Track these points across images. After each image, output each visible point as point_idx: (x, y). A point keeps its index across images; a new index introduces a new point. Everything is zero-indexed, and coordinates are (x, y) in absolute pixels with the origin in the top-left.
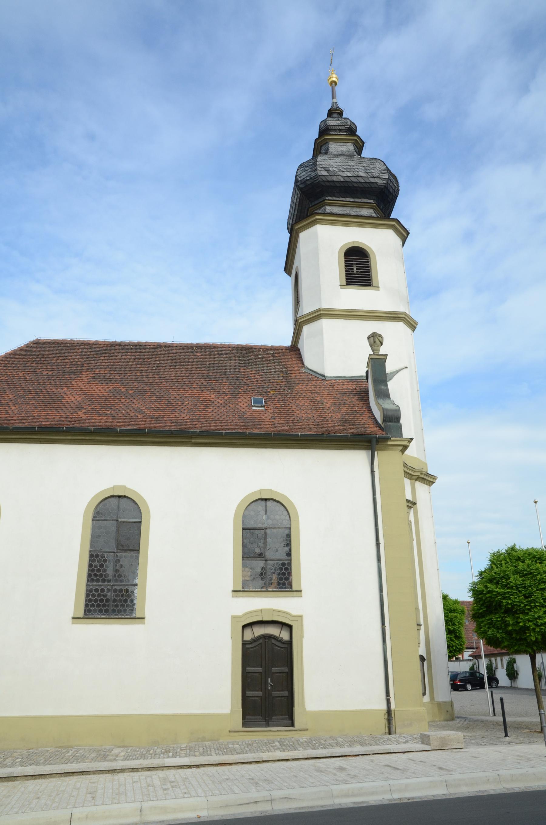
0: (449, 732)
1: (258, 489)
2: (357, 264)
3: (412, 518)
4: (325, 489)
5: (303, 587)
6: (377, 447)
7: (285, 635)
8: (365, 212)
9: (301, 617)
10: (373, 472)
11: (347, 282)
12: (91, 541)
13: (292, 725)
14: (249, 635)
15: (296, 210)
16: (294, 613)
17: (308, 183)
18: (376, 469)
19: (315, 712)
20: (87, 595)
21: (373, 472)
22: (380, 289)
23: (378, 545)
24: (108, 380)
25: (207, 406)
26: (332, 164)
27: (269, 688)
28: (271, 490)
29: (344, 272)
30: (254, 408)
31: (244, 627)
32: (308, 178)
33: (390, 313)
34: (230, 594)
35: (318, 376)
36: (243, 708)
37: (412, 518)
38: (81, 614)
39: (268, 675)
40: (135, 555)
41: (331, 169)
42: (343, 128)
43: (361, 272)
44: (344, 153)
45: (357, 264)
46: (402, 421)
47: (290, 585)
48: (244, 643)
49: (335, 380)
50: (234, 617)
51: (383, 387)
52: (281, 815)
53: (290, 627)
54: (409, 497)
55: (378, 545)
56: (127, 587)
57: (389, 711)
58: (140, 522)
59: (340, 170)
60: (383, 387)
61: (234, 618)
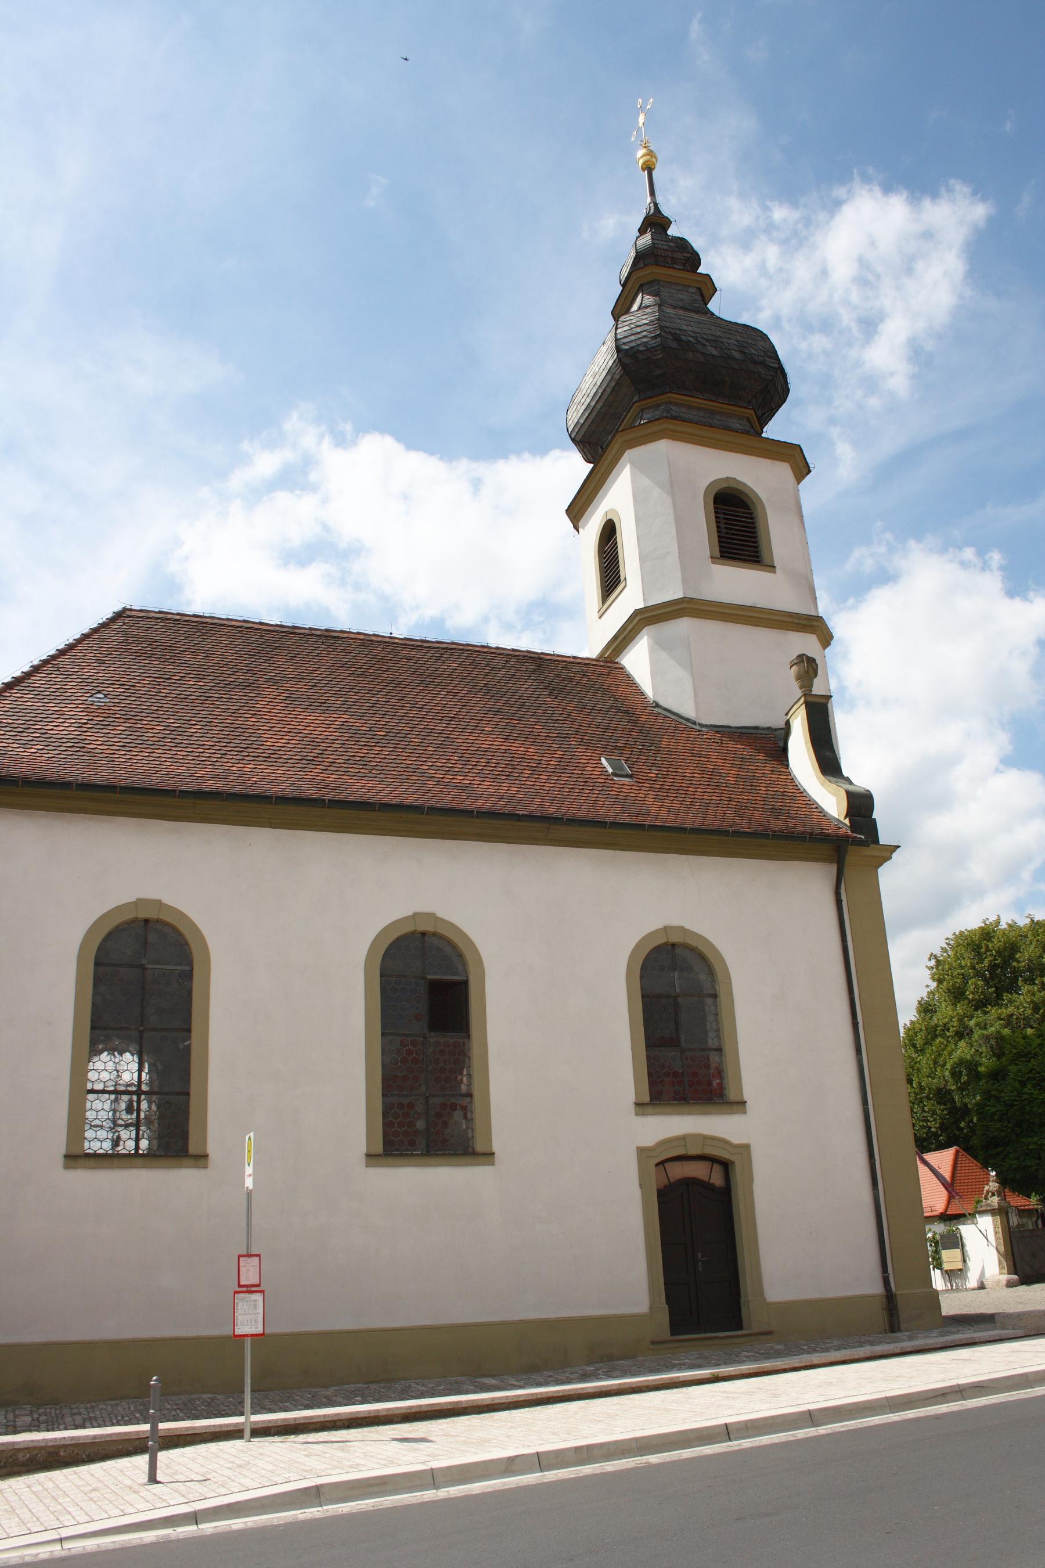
1: (660, 926)
2: (725, 519)
4: (760, 926)
8: (735, 424)
9: (747, 1147)
11: (721, 551)
12: (650, 1075)
13: (739, 1326)
15: (603, 400)
16: (736, 1141)
17: (641, 357)
18: (843, 897)
19: (779, 1303)
20: (385, 1115)
22: (778, 570)
26: (685, 327)
27: (701, 1269)
28: (683, 928)
32: (641, 348)
34: (632, 1108)
36: (667, 1303)
38: (380, 1149)
40: (461, 1041)
43: (732, 529)
44: (687, 306)
45: (725, 519)
48: (661, 1193)
51: (827, 753)
52: (668, 1463)
56: (453, 1100)
57: (890, 1297)
59: (699, 342)
60: (827, 753)
61: (642, 1151)
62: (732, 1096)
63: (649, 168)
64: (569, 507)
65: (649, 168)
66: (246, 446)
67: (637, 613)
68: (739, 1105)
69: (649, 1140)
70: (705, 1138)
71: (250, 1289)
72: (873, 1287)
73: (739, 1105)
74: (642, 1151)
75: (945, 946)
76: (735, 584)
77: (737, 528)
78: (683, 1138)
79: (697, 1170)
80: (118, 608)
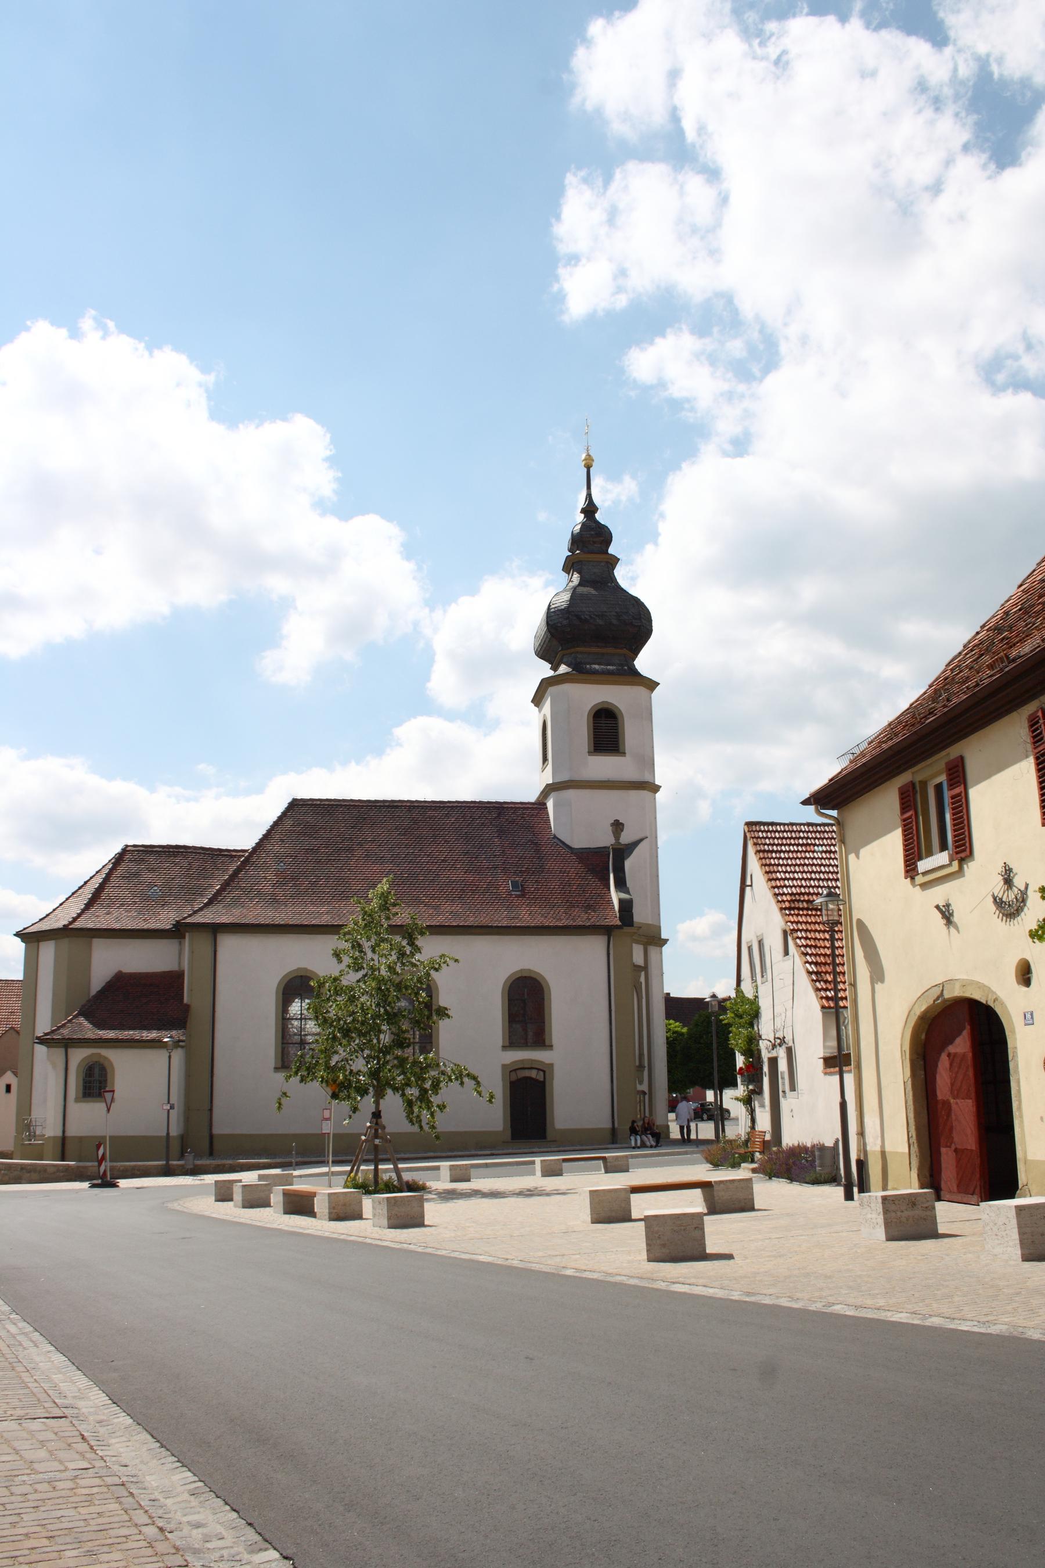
3: (642, 979)
4: (574, 972)
7: (541, 1078)
9: (552, 1065)
14: (514, 1078)
18: (611, 952)
37: (642, 979)
48: (511, 1083)
57: (613, 1129)
61: (504, 1066)
62: (547, 1043)
63: (588, 467)
64: (149, 850)
65: (588, 467)
66: (565, 622)
67: (548, 785)
68: (550, 1047)
69: (508, 1062)
70: (532, 1061)
71: (327, 1119)
72: (609, 1125)
73: (550, 1047)
74: (504, 1066)
75: (299, 1077)
76: (604, 766)
77: (606, 731)
78: (522, 1061)
79: (533, 1074)
80: (290, 800)
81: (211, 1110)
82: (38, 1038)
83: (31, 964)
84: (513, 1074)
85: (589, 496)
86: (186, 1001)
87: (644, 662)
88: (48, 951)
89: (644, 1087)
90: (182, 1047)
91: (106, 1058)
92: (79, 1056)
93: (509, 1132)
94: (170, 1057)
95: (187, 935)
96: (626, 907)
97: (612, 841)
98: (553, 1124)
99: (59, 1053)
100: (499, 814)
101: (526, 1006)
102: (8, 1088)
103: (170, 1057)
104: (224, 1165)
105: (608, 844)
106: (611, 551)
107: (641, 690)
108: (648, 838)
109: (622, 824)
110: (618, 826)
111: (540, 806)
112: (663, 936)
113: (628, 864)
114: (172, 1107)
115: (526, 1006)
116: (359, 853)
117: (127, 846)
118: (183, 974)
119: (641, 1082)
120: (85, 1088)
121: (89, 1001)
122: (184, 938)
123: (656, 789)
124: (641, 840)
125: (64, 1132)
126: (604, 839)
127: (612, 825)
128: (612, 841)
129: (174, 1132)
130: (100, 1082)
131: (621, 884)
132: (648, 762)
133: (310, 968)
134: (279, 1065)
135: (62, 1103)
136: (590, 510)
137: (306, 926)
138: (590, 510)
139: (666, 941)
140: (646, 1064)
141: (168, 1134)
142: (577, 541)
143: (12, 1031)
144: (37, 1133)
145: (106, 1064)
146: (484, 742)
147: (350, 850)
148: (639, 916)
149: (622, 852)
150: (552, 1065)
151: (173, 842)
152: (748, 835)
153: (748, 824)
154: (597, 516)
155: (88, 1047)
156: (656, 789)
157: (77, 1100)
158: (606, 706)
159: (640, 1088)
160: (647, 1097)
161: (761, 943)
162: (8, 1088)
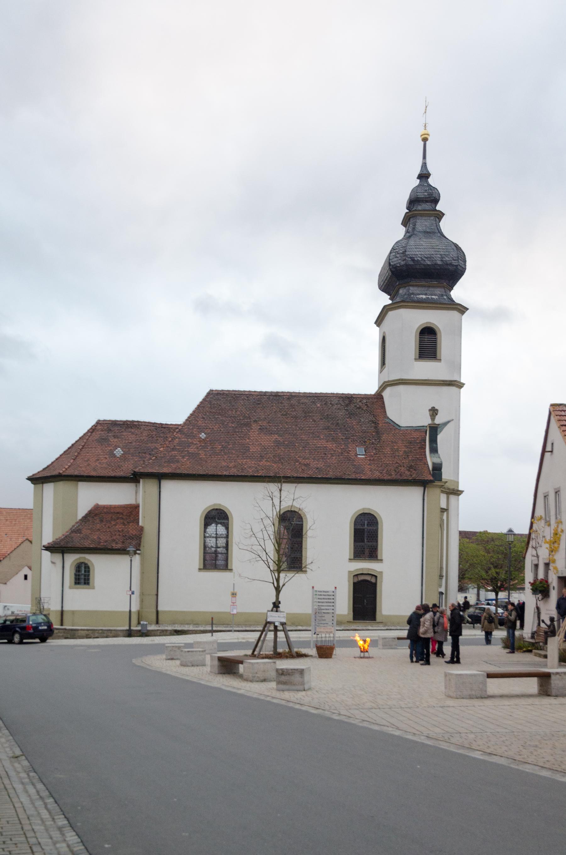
0: (560, 780)
3: (445, 517)
4: (398, 510)
5: (384, 558)
6: (427, 486)
7: (373, 580)
10: (424, 499)
13: (375, 620)
14: (356, 580)
16: (378, 570)
18: (426, 498)
21: (424, 499)
22: (442, 361)
23: (423, 538)
24: (271, 433)
25: (332, 455)
26: (417, 253)
29: (418, 345)
30: (359, 456)
31: (354, 576)
32: (398, 265)
33: (446, 381)
35: (395, 425)
37: (445, 517)
39: (365, 599)
41: (416, 259)
42: (429, 199)
46: (443, 470)
47: (377, 557)
48: (354, 584)
49: (407, 430)
50: (349, 572)
53: (376, 577)
54: (444, 506)
55: (423, 538)
58: (302, 524)
61: (350, 572)
62: (379, 558)
64: (114, 423)
66: (403, 263)
69: (352, 569)
74: (350, 572)
77: (428, 343)
81: (157, 595)
82: (44, 546)
83: (39, 499)
84: (356, 578)
85: (424, 165)
86: (140, 524)
87: (458, 293)
88: (49, 489)
89: (442, 590)
90: (139, 554)
91: (89, 560)
92: (71, 559)
93: (351, 616)
94: (131, 561)
95: (141, 481)
96: (438, 468)
97: (430, 421)
98: (381, 611)
99: (58, 558)
100: (350, 402)
101: (366, 535)
102: (26, 577)
103: (131, 561)
104: (166, 631)
105: (426, 424)
106: (438, 208)
107: (455, 313)
108: (454, 420)
109: (437, 410)
110: (434, 412)
111: (378, 397)
112: (460, 488)
113: (440, 437)
114: (133, 593)
115: (366, 535)
116: (255, 426)
117: (99, 421)
118: (139, 506)
119: (440, 586)
120: (76, 579)
121: (77, 523)
122: (139, 482)
123: (460, 385)
124: (449, 422)
125: (62, 607)
126: (425, 421)
127: (430, 410)
128: (430, 421)
129: (134, 609)
130: (85, 576)
131: (434, 450)
132: (458, 367)
133: (222, 504)
134: (202, 567)
135: (61, 589)
136: (424, 176)
137: (220, 475)
138: (424, 176)
139: (462, 492)
140: (444, 574)
141: (130, 611)
142: (413, 202)
143: (27, 541)
144: (45, 607)
145: (90, 565)
146: (340, 351)
147: (248, 425)
148: (446, 475)
149: (434, 430)
150: (381, 573)
151: (130, 418)
152: (552, 413)
153: (552, 405)
154: (431, 181)
155: (79, 553)
156: (460, 385)
157: (70, 588)
158: (429, 325)
159: (440, 590)
160: (444, 596)
161: (557, 492)
162: (26, 577)
